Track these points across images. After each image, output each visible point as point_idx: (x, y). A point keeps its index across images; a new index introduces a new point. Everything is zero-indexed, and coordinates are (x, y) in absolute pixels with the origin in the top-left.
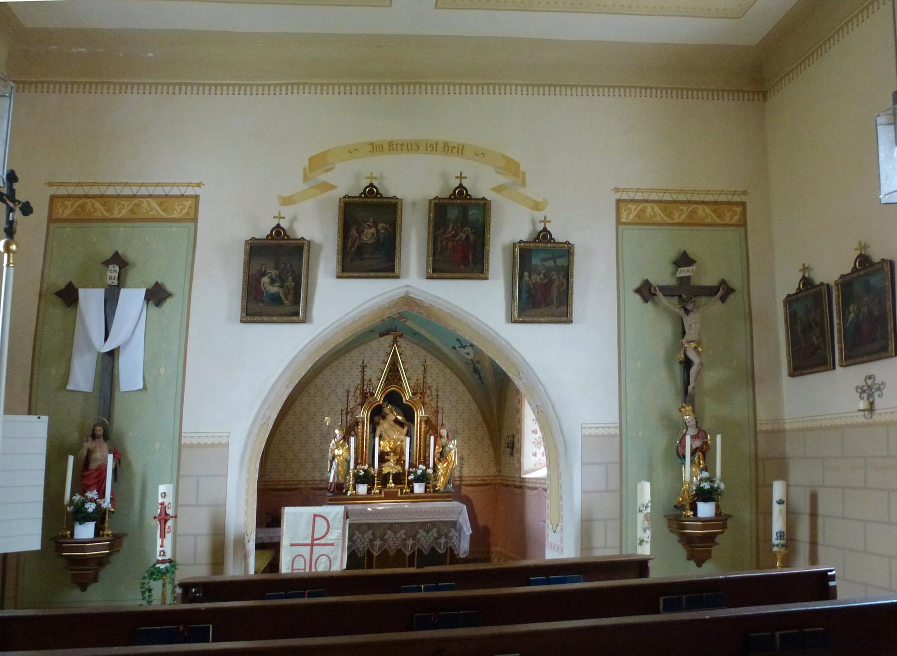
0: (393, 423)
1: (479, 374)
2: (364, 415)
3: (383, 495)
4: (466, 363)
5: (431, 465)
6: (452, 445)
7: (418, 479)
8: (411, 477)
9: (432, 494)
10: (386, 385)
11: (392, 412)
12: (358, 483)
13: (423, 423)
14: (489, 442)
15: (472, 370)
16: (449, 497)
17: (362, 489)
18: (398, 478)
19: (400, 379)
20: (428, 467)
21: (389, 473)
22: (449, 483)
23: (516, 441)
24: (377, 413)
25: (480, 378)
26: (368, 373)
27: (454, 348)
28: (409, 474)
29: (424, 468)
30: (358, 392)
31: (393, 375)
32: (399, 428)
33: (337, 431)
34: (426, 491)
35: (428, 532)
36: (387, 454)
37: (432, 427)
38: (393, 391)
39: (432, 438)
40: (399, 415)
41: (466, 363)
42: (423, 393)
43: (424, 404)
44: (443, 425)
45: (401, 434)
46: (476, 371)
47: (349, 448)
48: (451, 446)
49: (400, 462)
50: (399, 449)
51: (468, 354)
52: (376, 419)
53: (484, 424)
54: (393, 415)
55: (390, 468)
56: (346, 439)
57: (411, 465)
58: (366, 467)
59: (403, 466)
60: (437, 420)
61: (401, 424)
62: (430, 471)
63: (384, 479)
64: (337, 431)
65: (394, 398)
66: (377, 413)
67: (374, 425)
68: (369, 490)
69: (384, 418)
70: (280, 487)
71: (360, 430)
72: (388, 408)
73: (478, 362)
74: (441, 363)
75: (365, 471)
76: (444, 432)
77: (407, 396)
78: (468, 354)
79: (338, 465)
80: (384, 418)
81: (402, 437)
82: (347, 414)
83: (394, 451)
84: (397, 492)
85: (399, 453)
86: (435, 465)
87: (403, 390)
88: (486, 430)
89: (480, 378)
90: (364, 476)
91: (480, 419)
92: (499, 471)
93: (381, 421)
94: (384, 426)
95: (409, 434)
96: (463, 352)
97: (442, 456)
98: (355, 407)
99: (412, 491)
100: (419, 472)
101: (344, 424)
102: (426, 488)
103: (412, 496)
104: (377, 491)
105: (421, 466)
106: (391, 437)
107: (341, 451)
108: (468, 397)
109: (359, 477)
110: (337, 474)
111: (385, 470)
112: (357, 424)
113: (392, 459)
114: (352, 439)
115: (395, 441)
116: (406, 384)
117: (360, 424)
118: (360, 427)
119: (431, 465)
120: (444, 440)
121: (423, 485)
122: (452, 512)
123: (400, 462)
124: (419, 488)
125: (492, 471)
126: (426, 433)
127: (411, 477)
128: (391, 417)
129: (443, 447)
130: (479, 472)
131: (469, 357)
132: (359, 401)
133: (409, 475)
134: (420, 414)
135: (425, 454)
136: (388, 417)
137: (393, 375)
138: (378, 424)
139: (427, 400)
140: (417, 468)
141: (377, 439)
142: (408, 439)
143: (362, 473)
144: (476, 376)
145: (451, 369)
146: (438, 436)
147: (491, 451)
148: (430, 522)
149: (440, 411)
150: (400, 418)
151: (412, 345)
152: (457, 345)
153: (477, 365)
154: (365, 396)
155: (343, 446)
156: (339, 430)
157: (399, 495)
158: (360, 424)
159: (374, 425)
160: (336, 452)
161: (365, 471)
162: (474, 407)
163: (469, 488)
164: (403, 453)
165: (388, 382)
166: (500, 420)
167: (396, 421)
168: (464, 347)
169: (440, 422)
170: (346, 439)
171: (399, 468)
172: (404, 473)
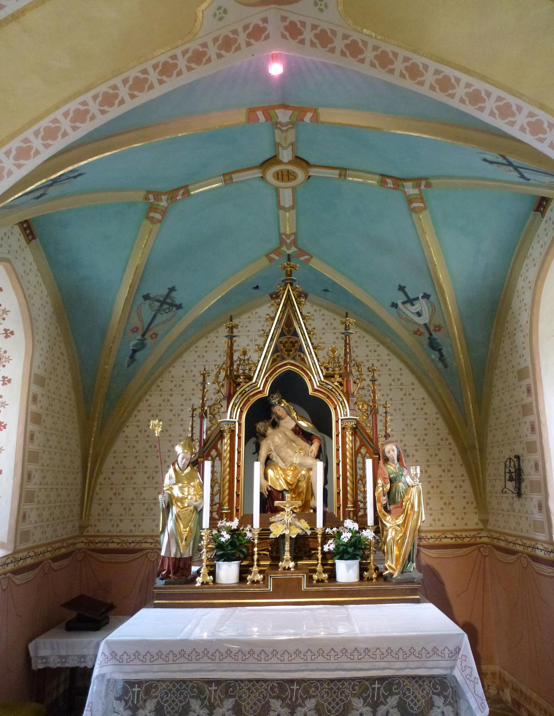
0: (291, 435)
1: (440, 351)
2: (234, 416)
3: (270, 588)
4: (416, 333)
5: (370, 520)
6: (412, 479)
7: (347, 552)
8: (330, 546)
9: (376, 587)
10: (274, 361)
11: (289, 414)
12: (220, 558)
13: (348, 433)
14: (463, 470)
15: (426, 345)
16: (413, 591)
17: (228, 572)
18: (303, 547)
19: (301, 350)
20: (363, 526)
21: (283, 536)
22: (410, 559)
23: (527, 467)
24: (261, 415)
25: (441, 357)
26: (240, 343)
27: (395, 305)
28: (326, 537)
29: (356, 526)
30: (223, 374)
31: (288, 343)
32: (301, 442)
33: (179, 449)
34: (361, 577)
35: (375, 706)
36: (281, 495)
37: (367, 442)
38: (289, 372)
39: (369, 463)
40: (304, 419)
41: (416, 333)
42: (345, 375)
43: (348, 395)
44: (387, 436)
45: (307, 455)
46: (433, 345)
47: (202, 486)
48: (408, 480)
49: (306, 511)
50: (303, 484)
51: (419, 314)
52: (260, 426)
53: (451, 440)
54: (290, 418)
55: (285, 525)
56: (196, 465)
57: (328, 519)
58: (234, 524)
59: (312, 522)
60: (375, 427)
61: (308, 437)
62: (368, 534)
63: (274, 549)
64: (179, 449)
65: (289, 387)
66: (261, 415)
67: (254, 436)
68: (244, 572)
69: (275, 425)
70: (111, 546)
71: (226, 448)
72: (280, 408)
73: (438, 328)
74: (370, 339)
75: (232, 532)
76: (391, 450)
77: (314, 381)
78: (419, 314)
79: (178, 518)
80: (275, 425)
81: (310, 461)
82: (202, 418)
83: (294, 488)
84: (299, 581)
85: (302, 491)
86: (377, 519)
87: (306, 369)
88: (455, 450)
89: (441, 357)
90: (231, 543)
91: (444, 431)
92: (485, 522)
93: (270, 431)
94: (275, 440)
95: (321, 455)
96: (410, 310)
97: (392, 499)
98: (218, 403)
99: (332, 576)
100: (346, 537)
101: (197, 436)
102: (363, 569)
103: (331, 591)
104: (260, 577)
105: (349, 524)
106: (290, 458)
107: (185, 495)
108: (420, 393)
109: (220, 546)
110: (175, 536)
111: (276, 531)
112: (221, 435)
113: (288, 504)
114: (208, 465)
115: (296, 468)
116: (312, 359)
117: (227, 436)
118: (226, 440)
119: (370, 520)
120: (392, 468)
121: (355, 564)
122: (435, 650)
123: (306, 511)
124: (346, 572)
125: (473, 520)
126: (356, 452)
127: (330, 546)
128: (288, 424)
129: (392, 481)
130: (448, 522)
131: (424, 319)
132: (224, 390)
133: (324, 542)
134: (341, 413)
135: (355, 495)
136: (282, 423)
137: (288, 343)
138: (264, 436)
139: (353, 388)
140: (340, 524)
141: (258, 467)
142: (320, 465)
143: (226, 537)
144: (435, 355)
145: (388, 348)
146: (380, 459)
147: (467, 486)
148: (381, 679)
149: (381, 410)
150: (303, 424)
151: (324, 311)
152: (400, 298)
153: (435, 335)
154: (235, 379)
155: (190, 478)
156: (184, 447)
157: (304, 587)
158: (227, 436)
159: (254, 436)
160: (176, 492)
161: (232, 532)
162: (431, 409)
163: (433, 553)
164: (311, 492)
165: (279, 353)
166: (482, 435)
167: (298, 431)
168: (411, 301)
169: (381, 433)
170: (196, 465)
171: (304, 525)
172: (314, 535)
